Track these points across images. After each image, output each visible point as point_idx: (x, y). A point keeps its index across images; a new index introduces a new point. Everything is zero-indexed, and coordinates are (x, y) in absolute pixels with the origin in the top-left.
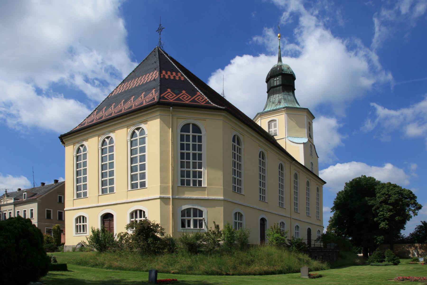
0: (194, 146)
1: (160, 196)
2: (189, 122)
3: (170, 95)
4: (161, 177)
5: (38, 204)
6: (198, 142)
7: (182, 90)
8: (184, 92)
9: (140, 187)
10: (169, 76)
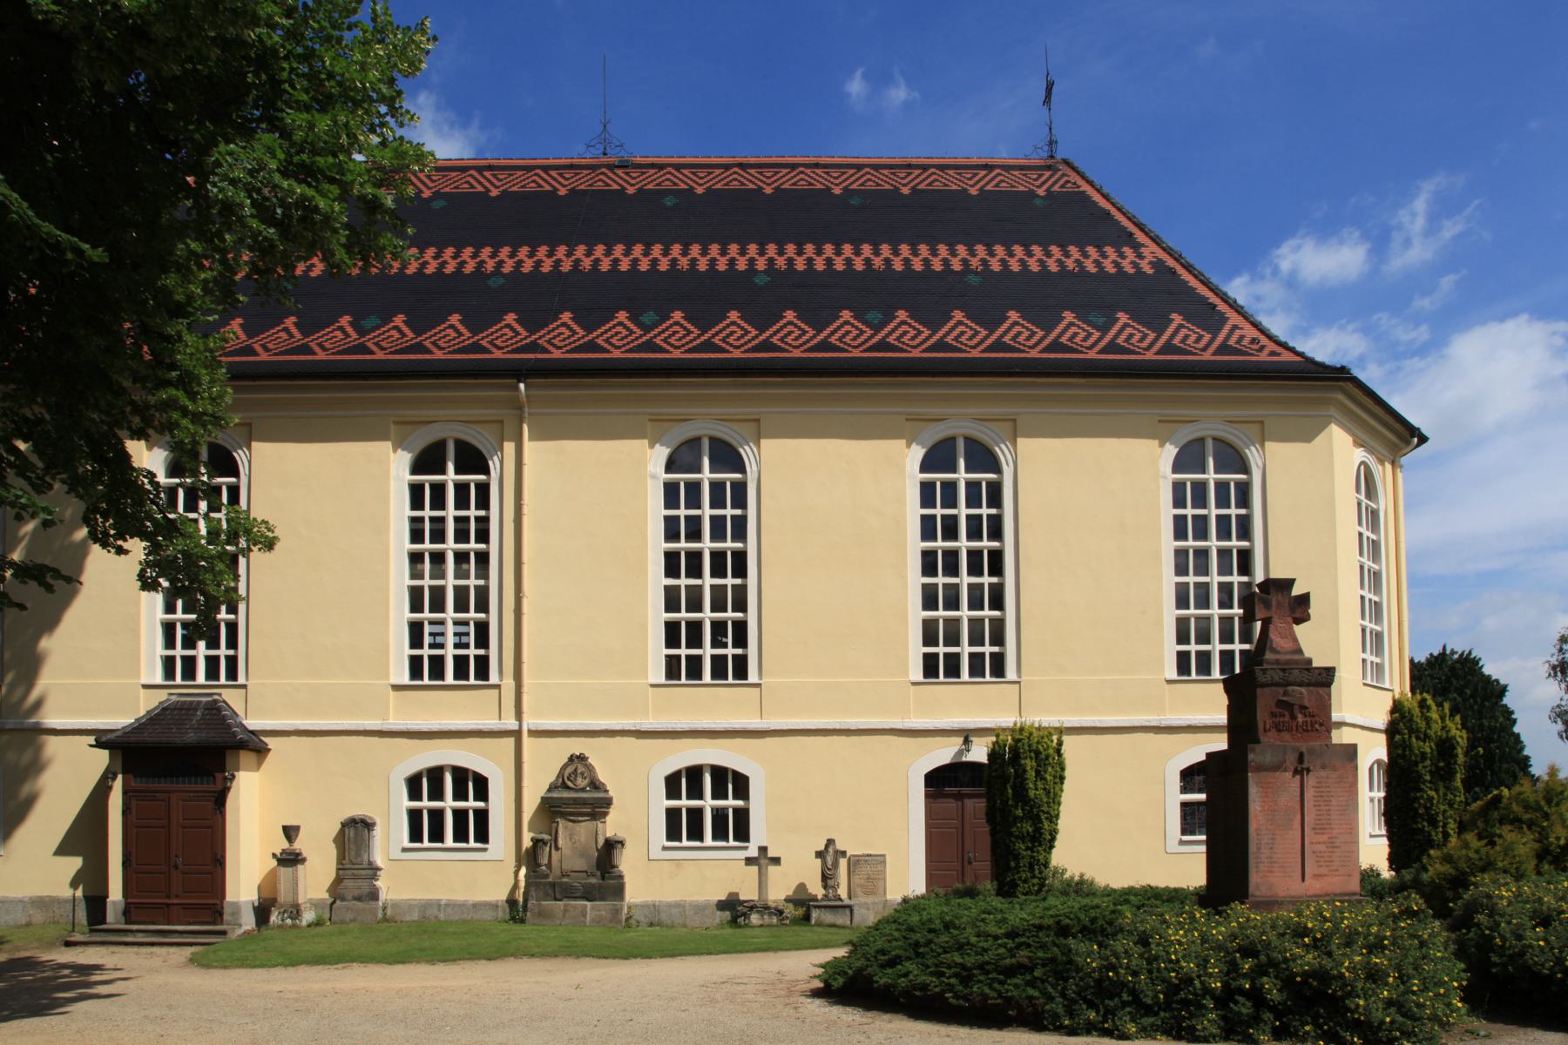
0: (717, 523)
2: (726, 433)
3: (908, 332)
5: (1210, 844)
6: (687, 507)
7: (897, 309)
8: (902, 315)
10: (926, 262)
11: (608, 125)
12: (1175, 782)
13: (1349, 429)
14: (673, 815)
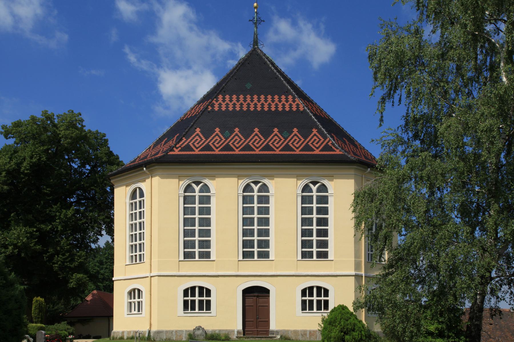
1: (355, 273)
4: (355, 250)
9: (199, 258)
11: (258, 36)
12: (126, 295)
13: (122, 185)
14: (304, 302)
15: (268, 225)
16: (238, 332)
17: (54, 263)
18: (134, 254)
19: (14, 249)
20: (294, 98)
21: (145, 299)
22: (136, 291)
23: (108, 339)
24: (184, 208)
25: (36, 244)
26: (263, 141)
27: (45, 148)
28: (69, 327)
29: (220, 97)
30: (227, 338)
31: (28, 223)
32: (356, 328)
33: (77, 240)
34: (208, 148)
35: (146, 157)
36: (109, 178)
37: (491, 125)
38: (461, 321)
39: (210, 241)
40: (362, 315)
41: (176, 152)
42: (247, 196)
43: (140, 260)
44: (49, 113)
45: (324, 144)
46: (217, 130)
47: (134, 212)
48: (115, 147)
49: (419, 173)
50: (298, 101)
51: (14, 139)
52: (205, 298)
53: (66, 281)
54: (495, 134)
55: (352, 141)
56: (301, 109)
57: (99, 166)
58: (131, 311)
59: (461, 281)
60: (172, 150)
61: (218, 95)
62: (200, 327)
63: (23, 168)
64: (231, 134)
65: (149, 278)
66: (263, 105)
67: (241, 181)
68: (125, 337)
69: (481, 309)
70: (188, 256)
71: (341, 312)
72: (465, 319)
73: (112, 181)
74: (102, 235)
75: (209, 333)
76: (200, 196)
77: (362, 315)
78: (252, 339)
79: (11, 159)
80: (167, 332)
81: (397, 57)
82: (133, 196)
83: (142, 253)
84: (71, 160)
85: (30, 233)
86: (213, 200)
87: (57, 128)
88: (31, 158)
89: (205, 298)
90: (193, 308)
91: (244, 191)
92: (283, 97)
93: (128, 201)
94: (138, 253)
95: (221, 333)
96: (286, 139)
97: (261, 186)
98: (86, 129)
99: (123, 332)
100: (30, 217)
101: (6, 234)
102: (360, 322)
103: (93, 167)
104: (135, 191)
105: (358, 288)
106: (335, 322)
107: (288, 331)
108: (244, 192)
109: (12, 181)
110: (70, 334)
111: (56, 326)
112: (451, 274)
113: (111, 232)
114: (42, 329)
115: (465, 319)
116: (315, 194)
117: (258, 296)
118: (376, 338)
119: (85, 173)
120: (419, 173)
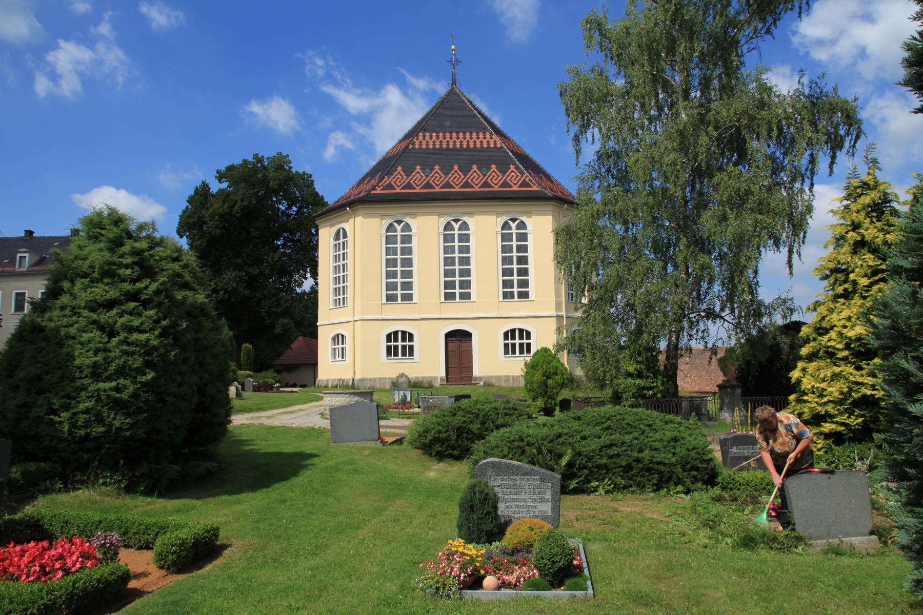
15: (469, 264)
16: (442, 379)
17: (262, 308)
18: (338, 297)
19: (225, 294)
20: (491, 135)
21: (348, 345)
22: (340, 336)
23: (313, 388)
24: (387, 248)
25: (341, 149)
26: (463, 179)
27: (255, 190)
28: (276, 375)
29: (421, 135)
30: (431, 386)
31: (239, 268)
32: (559, 372)
33: (282, 283)
34: (409, 186)
35: (349, 197)
36: (313, 220)
37: (675, 160)
38: (658, 360)
39: (411, 282)
40: (564, 357)
41: (379, 191)
42: (448, 234)
43: (344, 304)
44: (260, 156)
45: (522, 180)
46: (418, 168)
47: (338, 253)
48: (319, 188)
49: (612, 208)
50: (496, 137)
51: (227, 183)
52: (407, 343)
53: (272, 326)
54: (678, 167)
55: (548, 177)
56: (499, 146)
57: (305, 208)
58: (335, 358)
59: (656, 318)
60: (374, 189)
61: (419, 133)
62: (404, 374)
63: (234, 212)
64: (432, 171)
65: (352, 323)
66: (461, 142)
67: (441, 219)
68: (330, 386)
69: (676, 347)
70: (391, 298)
71: (543, 355)
72: (662, 358)
73: (317, 222)
74: (306, 278)
75: (413, 381)
76: (402, 236)
77: (564, 357)
78: (455, 386)
79: (224, 203)
80: (370, 379)
81: (586, 92)
82: (337, 237)
83: (345, 296)
84: (278, 202)
85: (240, 277)
86: (414, 239)
87: (267, 171)
88: (242, 201)
89: (407, 343)
90: (396, 354)
91: (445, 229)
92: (481, 134)
93: (332, 242)
94: (341, 297)
95: (425, 381)
96: (484, 176)
97: (461, 224)
98: (294, 171)
99: (328, 380)
100: (239, 261)
101: (218, 279)
102: (562, 365)
103: (299, 209)
104: (338, 232)
105: (559, 330)
106: (537, 365)
107: (491, 377)
108: (444, 230)
109: (224, 225)
110: (276, 382)
111: (264, 374)
112: (647, 312)
113: (315, 275)
114: (250, 376)
115: (662, 358)
116: (514, 231)
117: (460, 341)
118: (578, 382)
119: (291, 215)
120: (612, 208)
